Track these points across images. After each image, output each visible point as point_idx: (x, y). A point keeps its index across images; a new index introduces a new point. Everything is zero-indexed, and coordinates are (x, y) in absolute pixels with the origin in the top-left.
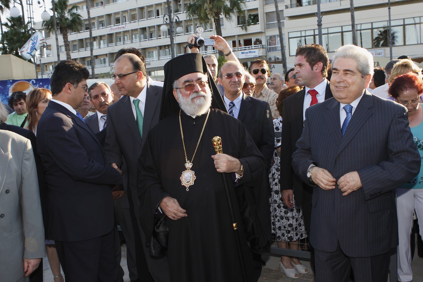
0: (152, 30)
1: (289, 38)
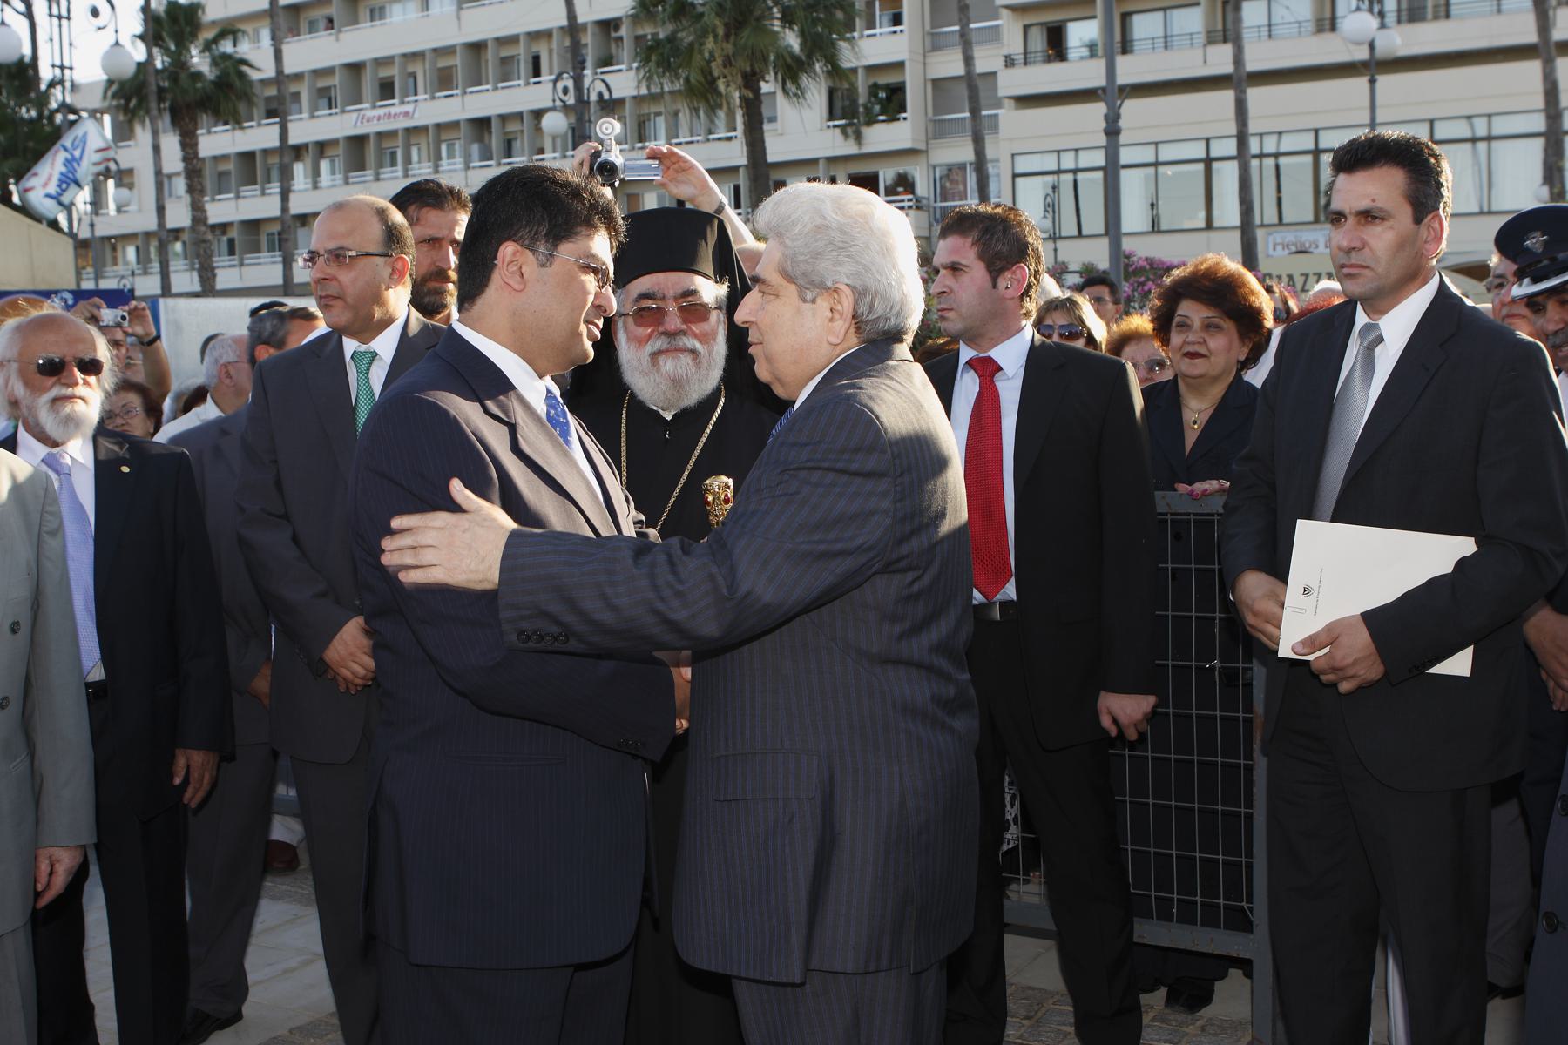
0: (512, 127)
1: (1015, 176)
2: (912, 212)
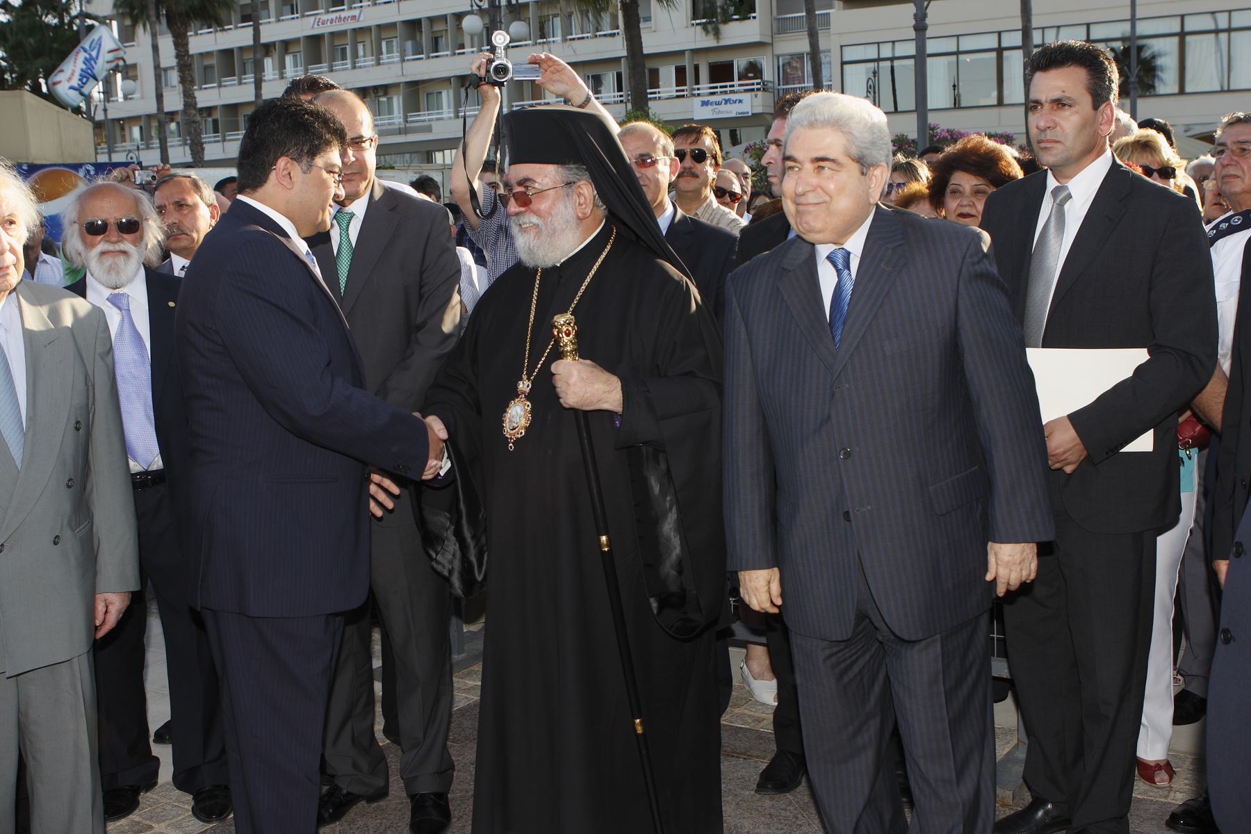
0: (438, 27)
1: (843, 63)
2: (760, 94)
